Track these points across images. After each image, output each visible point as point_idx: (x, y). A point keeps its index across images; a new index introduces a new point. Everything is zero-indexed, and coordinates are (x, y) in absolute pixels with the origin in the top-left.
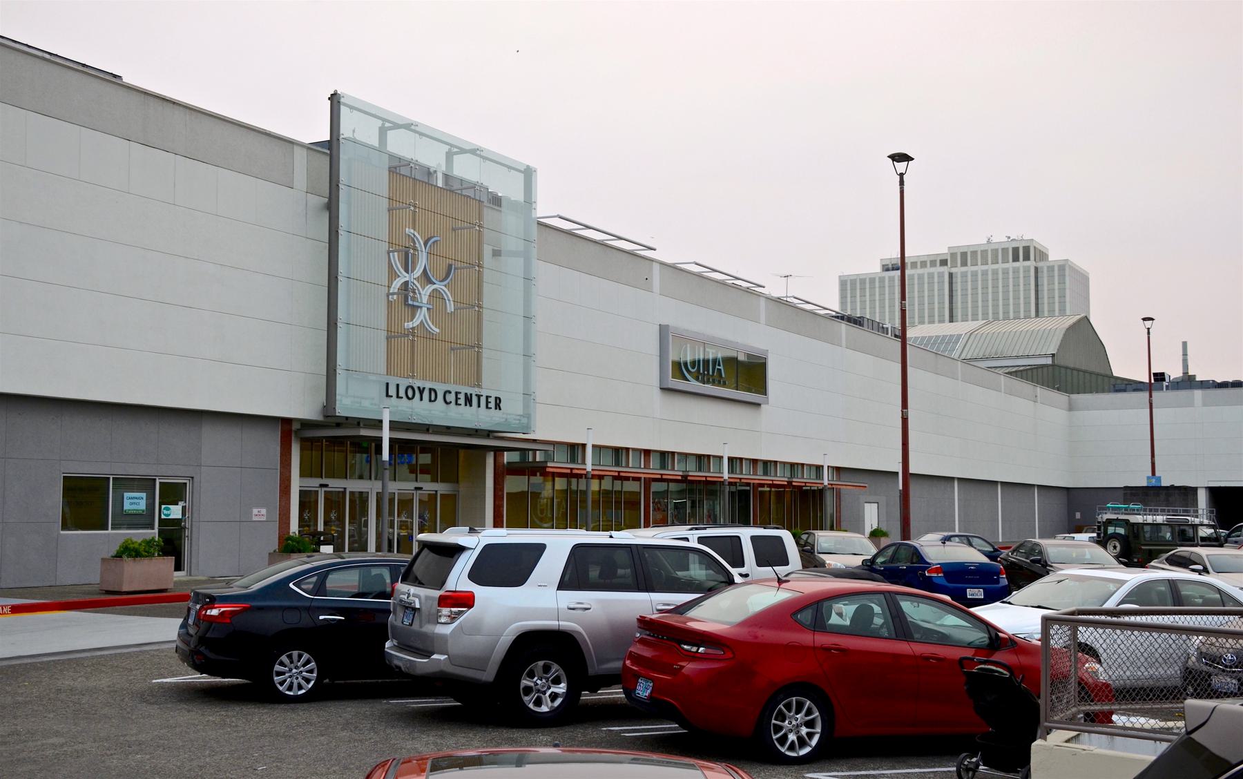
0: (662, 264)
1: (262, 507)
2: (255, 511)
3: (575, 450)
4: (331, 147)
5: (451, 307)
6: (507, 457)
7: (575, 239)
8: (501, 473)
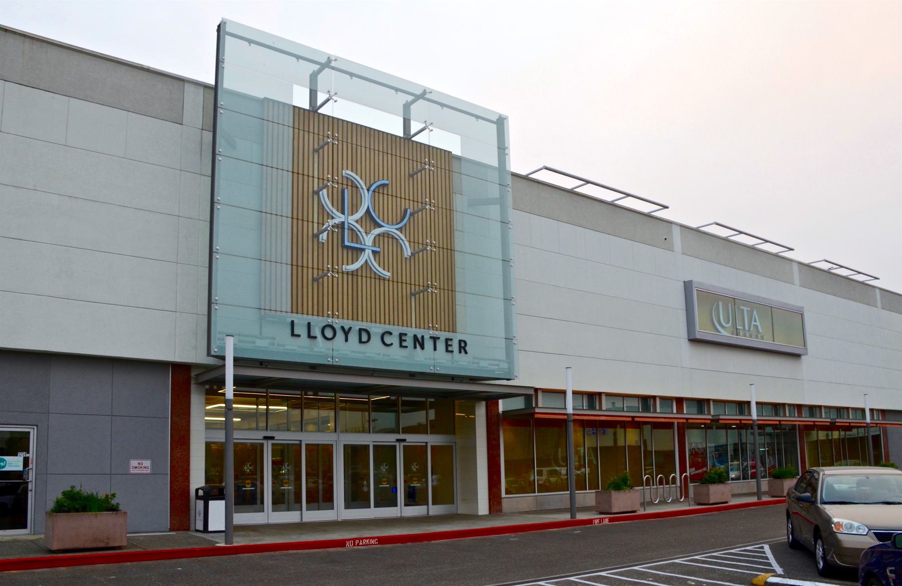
0: (800, 263)
1: (146, 458)
2: (134, 463)
3: (743, 406)
4: (215, 88)
5: (408, 252)
6: (502, 405)
7: (575, 197)
8: (494, 422)
